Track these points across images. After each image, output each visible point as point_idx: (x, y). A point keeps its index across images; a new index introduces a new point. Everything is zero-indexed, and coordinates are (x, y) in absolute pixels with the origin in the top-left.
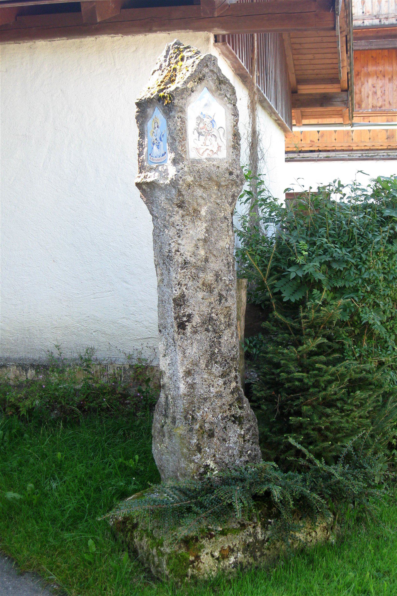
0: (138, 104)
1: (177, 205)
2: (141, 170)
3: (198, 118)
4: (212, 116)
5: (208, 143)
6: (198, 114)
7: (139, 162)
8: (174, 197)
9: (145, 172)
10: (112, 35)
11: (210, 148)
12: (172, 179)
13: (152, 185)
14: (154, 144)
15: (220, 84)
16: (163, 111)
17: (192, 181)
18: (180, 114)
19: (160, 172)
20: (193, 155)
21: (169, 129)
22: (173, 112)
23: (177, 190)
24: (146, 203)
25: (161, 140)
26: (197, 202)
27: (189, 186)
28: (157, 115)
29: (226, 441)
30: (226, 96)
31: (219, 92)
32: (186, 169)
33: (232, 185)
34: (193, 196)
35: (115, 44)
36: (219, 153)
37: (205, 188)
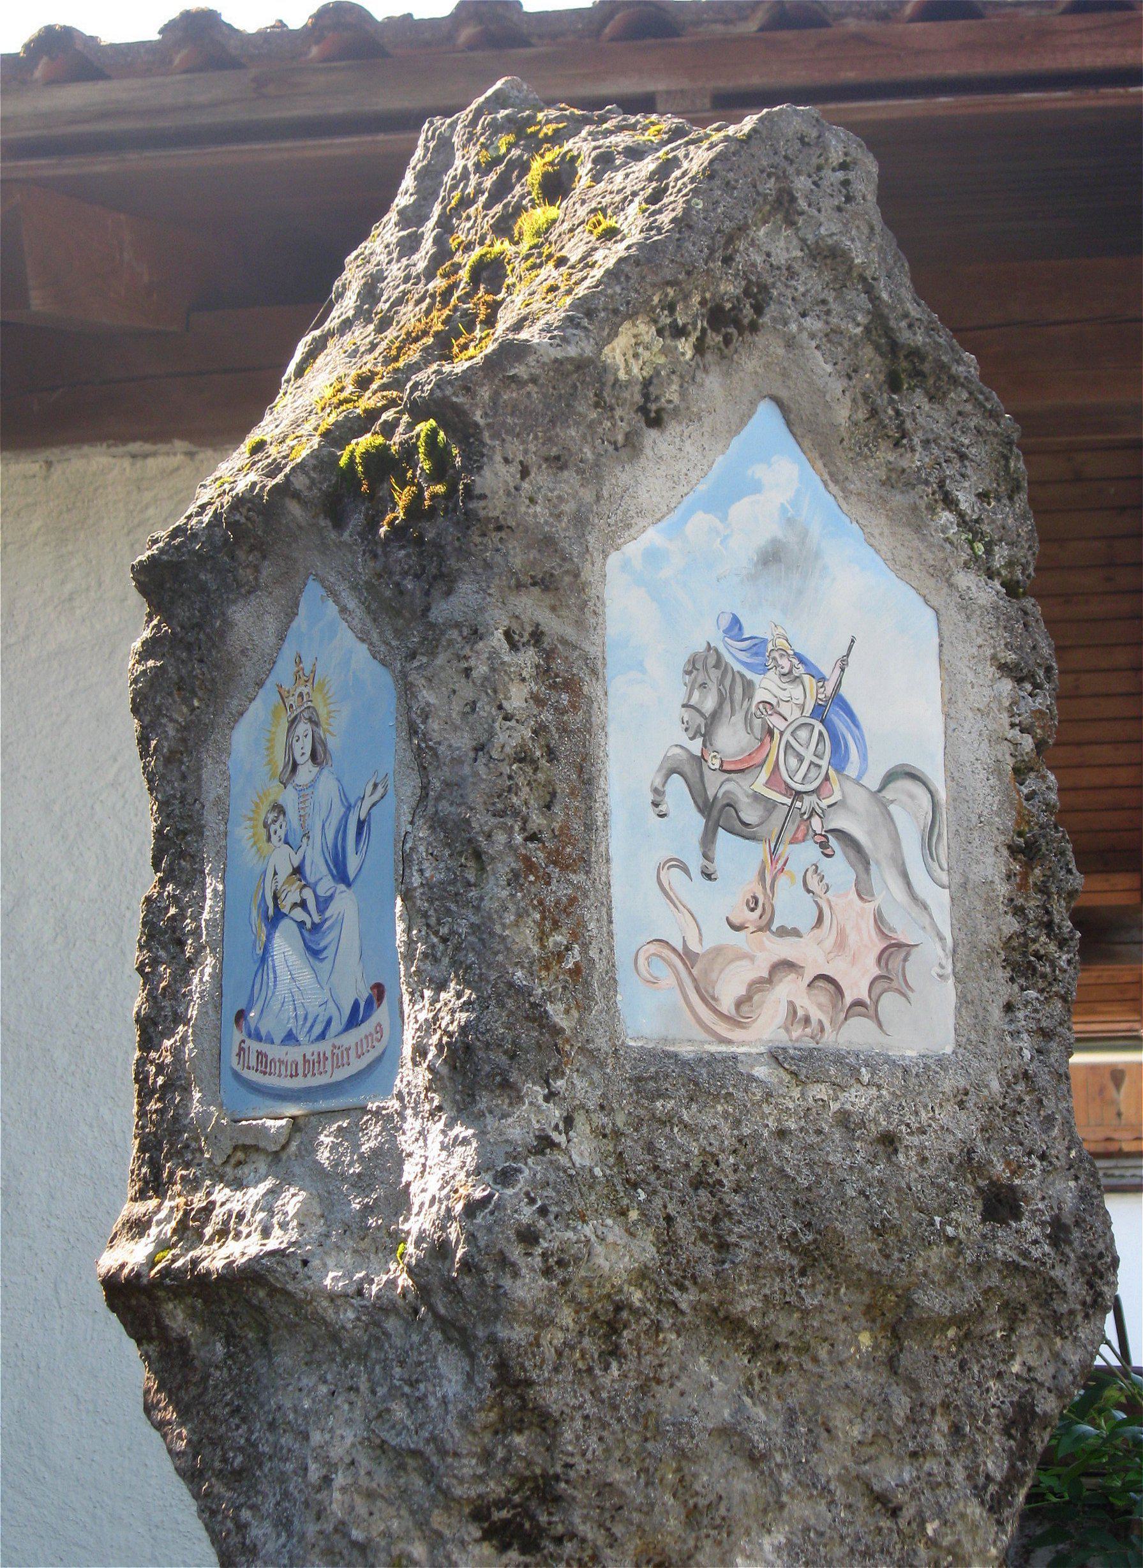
0: (159, 580)
1: (479, 1513)
2: (156, 1168)
3: (703, 666)
4: (826, 667)
5: (790, 903)
6: (705, 633)
7: (145, 1093)
8: (453, 1432)
9: (193, 1185)
10: (135, 447)
11: (812, 954)
12: (442, 1250)
13: (250, 1302)
14: (274, 919)
15: (894, 383)
16: (369, 592)
17: (642, 1276)
18: (531, 607)
19: (326, 1186)
20: (648, 1012)
21: (423, 755)
22: (466, 588)
23: (487, 1361)
24: (191, 1476)
25: (342, 876)
26: (683, 1486)
27: (613, 1328)
28: (322, 648)
30: (950, 502)
31: (885, 454)
32: (582, 1151)
33: (1013, 1313)
34: (649, 1425)
35: (148, 496)
36: (889, 1003)
37: (760, 1345)
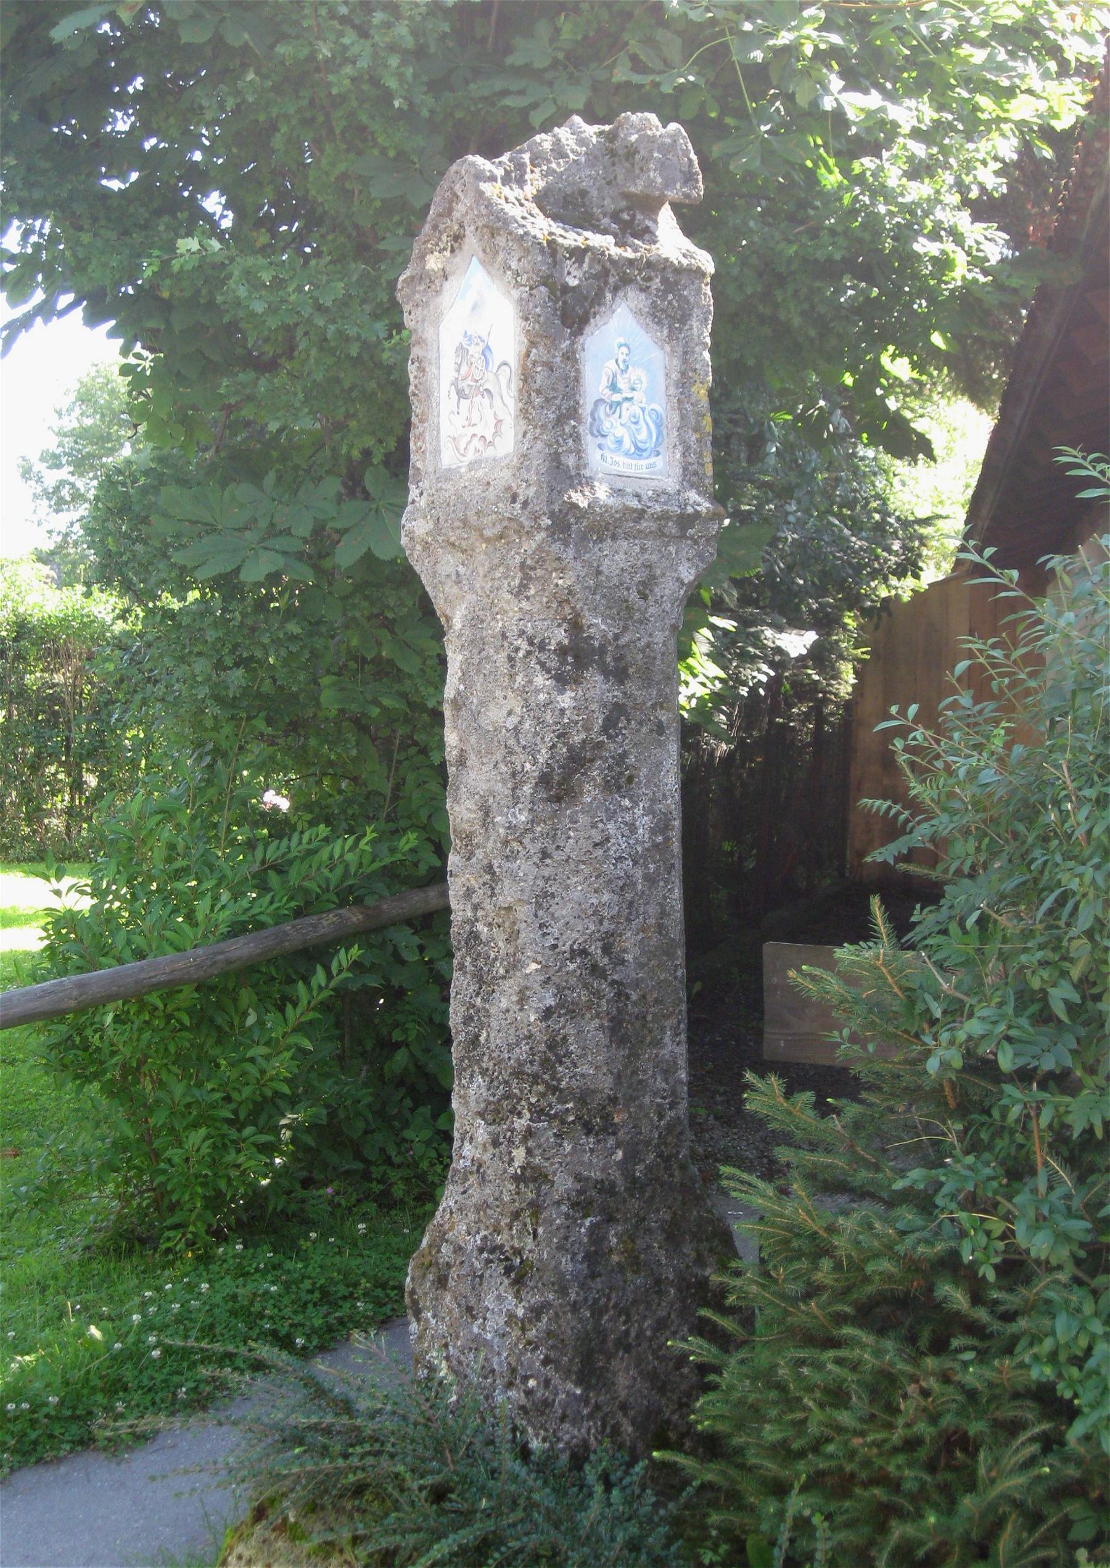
6: (460, 338)
29: (474, 1318)
